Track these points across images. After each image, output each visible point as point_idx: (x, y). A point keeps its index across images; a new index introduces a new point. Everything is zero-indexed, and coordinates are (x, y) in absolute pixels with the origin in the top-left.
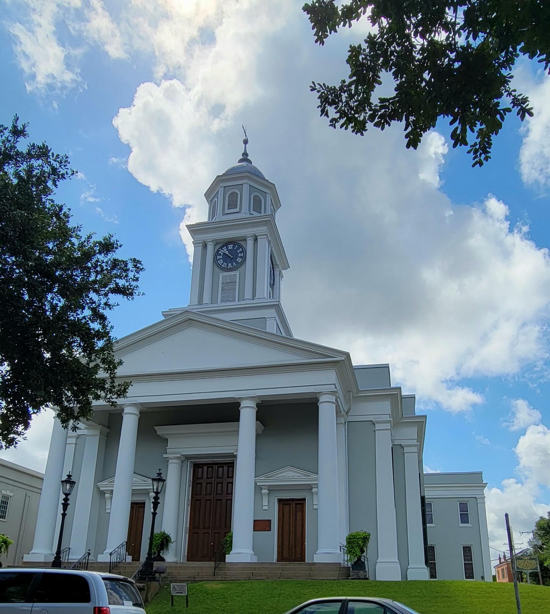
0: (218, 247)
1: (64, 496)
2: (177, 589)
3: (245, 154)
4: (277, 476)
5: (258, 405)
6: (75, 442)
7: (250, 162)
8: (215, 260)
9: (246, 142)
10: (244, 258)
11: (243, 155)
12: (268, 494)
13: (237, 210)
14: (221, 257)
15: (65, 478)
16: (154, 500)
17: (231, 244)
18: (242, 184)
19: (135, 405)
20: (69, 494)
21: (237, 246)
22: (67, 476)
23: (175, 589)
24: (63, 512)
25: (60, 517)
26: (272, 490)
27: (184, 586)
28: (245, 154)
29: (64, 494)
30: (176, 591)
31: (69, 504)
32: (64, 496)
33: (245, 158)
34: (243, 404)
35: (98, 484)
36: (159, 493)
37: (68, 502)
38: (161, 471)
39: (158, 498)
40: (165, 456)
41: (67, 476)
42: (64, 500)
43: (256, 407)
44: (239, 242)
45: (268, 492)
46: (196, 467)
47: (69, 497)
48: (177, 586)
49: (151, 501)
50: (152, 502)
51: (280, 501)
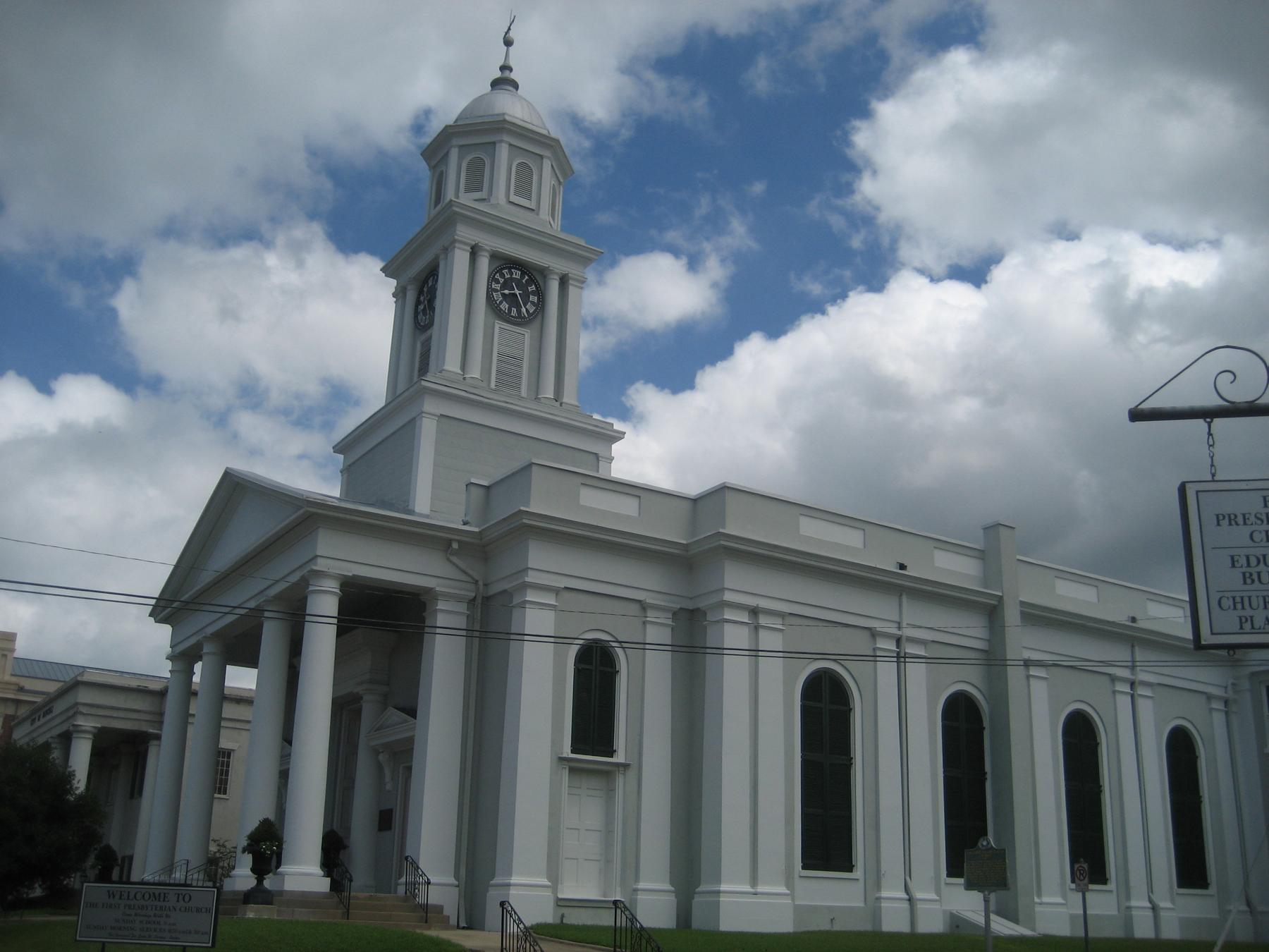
0: (497, 264)
10: (541, 305)
11: (503, 68)
13: (533, 205)
21: (527, 277)
27: (80, 937)
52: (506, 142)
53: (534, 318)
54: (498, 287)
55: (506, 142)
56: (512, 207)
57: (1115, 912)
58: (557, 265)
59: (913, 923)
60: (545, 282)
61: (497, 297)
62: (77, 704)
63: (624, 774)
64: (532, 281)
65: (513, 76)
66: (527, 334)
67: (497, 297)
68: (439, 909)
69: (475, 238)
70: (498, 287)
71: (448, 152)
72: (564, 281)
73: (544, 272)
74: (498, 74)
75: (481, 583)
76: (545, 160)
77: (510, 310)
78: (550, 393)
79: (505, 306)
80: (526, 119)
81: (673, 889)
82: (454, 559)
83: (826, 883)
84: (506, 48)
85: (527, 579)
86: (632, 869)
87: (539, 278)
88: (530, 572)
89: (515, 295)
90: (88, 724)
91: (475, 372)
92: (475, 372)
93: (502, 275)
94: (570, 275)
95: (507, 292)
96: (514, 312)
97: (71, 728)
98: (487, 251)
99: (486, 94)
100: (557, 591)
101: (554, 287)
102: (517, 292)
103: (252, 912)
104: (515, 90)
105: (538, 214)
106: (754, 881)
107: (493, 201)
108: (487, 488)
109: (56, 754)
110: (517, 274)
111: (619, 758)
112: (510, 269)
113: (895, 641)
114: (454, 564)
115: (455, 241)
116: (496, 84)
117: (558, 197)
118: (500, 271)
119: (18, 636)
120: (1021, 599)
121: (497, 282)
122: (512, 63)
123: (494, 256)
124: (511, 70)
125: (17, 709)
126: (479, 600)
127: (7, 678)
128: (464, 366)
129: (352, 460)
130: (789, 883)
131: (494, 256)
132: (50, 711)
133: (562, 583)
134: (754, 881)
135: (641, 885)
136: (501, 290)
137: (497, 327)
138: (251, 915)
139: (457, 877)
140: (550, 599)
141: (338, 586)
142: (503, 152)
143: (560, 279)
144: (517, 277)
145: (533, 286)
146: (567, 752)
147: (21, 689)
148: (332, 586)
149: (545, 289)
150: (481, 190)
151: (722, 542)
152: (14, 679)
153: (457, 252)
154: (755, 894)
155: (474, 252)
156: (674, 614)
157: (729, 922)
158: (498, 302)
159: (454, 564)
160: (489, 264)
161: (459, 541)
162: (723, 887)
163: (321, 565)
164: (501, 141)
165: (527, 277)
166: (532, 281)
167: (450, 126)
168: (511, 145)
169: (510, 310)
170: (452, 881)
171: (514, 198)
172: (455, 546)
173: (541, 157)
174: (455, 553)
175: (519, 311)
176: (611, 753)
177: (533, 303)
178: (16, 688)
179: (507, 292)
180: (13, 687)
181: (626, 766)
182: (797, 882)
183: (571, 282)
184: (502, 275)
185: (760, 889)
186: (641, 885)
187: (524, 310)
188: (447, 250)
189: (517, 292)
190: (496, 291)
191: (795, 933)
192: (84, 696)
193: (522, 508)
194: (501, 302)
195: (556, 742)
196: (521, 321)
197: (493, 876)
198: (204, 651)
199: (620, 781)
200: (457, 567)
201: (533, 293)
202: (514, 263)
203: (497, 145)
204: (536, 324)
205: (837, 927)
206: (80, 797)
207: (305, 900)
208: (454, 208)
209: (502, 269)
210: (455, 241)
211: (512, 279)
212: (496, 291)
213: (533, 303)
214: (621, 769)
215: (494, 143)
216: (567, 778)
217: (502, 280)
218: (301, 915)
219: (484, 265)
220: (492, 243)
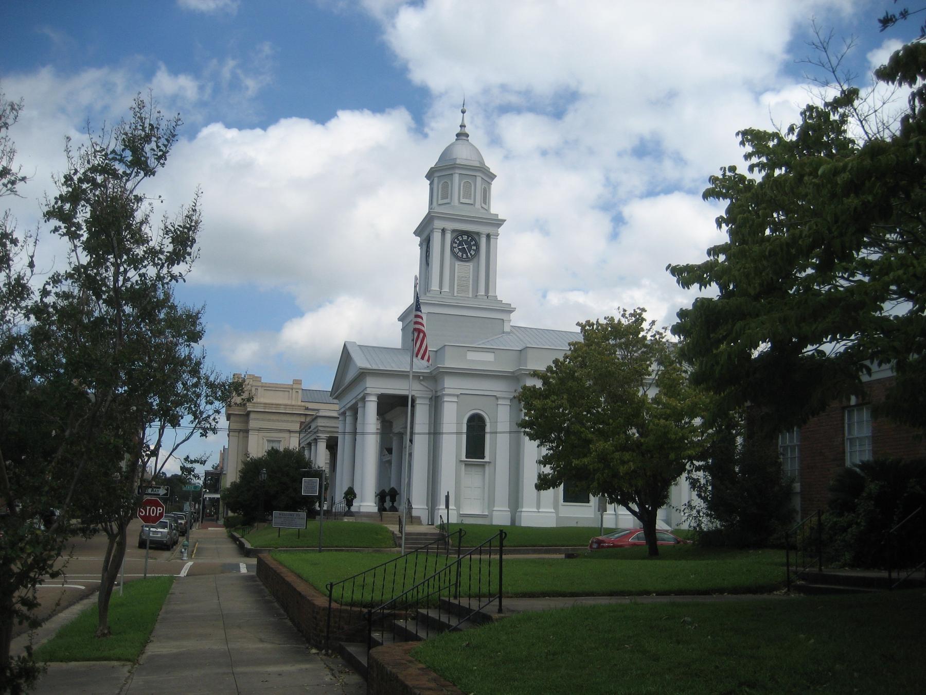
0: (455, 234)
3: (463, 126)
8: (452, 248)
10: (478, 250)
13: (471, 202)
21: (470, 238)
28: (463, 126)
38: (67, 136)
52: (457, 173)
53: (474, 257)
54: (456, 245)
55: (457, 173)
56: (462, 205)
57: (593, 516)
58: (484, 230)
59: (616, 524)
60: (479, 239)
61: (456, 250)
62: (317, 426)
63: (489, 465)
64: (473, 239)
65: (467, 130)
66: (470, 265)
67: (456, 250)
68: (419, 518)
70: (456, 245)
71: (433, 180)
72: (488, 236)
73: (478, 234)
74: (458, 130)
75: (434, 391)
76: (477, 177)
77: (462, 255)
78: (482, 292)
79: (460, 254)
80: (469, 158)
81: (509, 510)
82: (422, 383)
83: (580, 507)
85: (444, 392)
86: (491, 502)
88: (446, 389)
89: (464, 248)
90: (323, 436)
91: (446, 289)
92: (446, 289)
93: (458, 240)
95: (460, 247)
96: (465, 256)
97: (316, 437)
99: (452, 145)
100: (458, 396)
101: (483, 240)
102: (465, 246)
103: (346, 520)
104: (466, 138)
105: (474, 206)
106: (538, 506)
107: (452, 204)
108: (436, 351)
109: (306, 453)
110: (465, 237)
111: (487, 459)
112: (461, 236)
114: (422, 384)
115: (434, 229)
116: (458, 135)
119: (413, 231)
121: (456, 243)
123: (454, 231)
124: (465, 126)
125: (306, 418)
126: (433, 398)
127: (300, 403)
128: (441, 286)
129: (406, 323)
130: (556, 507)
132: (310, 427)
133: (459, 392)
134: (538, 506)
135: (495, 509)
136: (458, 247)
137: (456, 264)
138: (346, 520)
139: (427, 505)
140: (455, 399)
141: (377, 398)
142: (456, 178)
143: (487, 236)
146: (464, 458)
147: (307, 409)
148: (375, 399)
149: (480, 241)
150: (447, 198)
151: (523, 372)
152: (303, 404)
153: (435, 234)
154: (539, 512)
155: (443, 231)
156: (511, 400)
157: (524, 524)
159: (422, 384)
161: (423, 376)
162: (523, 510)
163: (368, 391)
164: (455, 173)
165: (470, 238)
167: (433, 168)
168: (482, 178)
169: (462, 255)
170: (426, 507)
171: (463, 200)
172: (421, 378)
174: (421, 380)
175: (467, 255)
176: (483, 457)
177: (474, 250)
178: (304, 408)
179: (460, 247)
180: (302, 408)
181: (489, 462)
182: (560, 507)
183: (492, 237)
184: (458, 240)
185: (540, 510)
186: (495, 509)
187: (469, 254)
188: (432, 231)
189: (465, 246)
190: (455, 247)
191: (556, 527)
192: (320, 422)
193: (439, 366)
194: (458, 252)
195: (458, 454)
196: (468, 260)
197: (437, 506)
198: (359, 406)
199: (487, 467)
200: (424, 386)
201: (474, 245)
203: (454, 175)
204: (475, 260)
205: (579, 525)
207: (368, 515)
208: (432, 214)
209: (457, 237)
210: (434, 229)
211: (463, 240)
212: (455, 247)
213: (474, 250)
214: (488, 464)
215: (452, 174)
216: (464, 470)
217: (458, 242)
218: (365, 520)
219: (449, 237)
220: (450, 226)
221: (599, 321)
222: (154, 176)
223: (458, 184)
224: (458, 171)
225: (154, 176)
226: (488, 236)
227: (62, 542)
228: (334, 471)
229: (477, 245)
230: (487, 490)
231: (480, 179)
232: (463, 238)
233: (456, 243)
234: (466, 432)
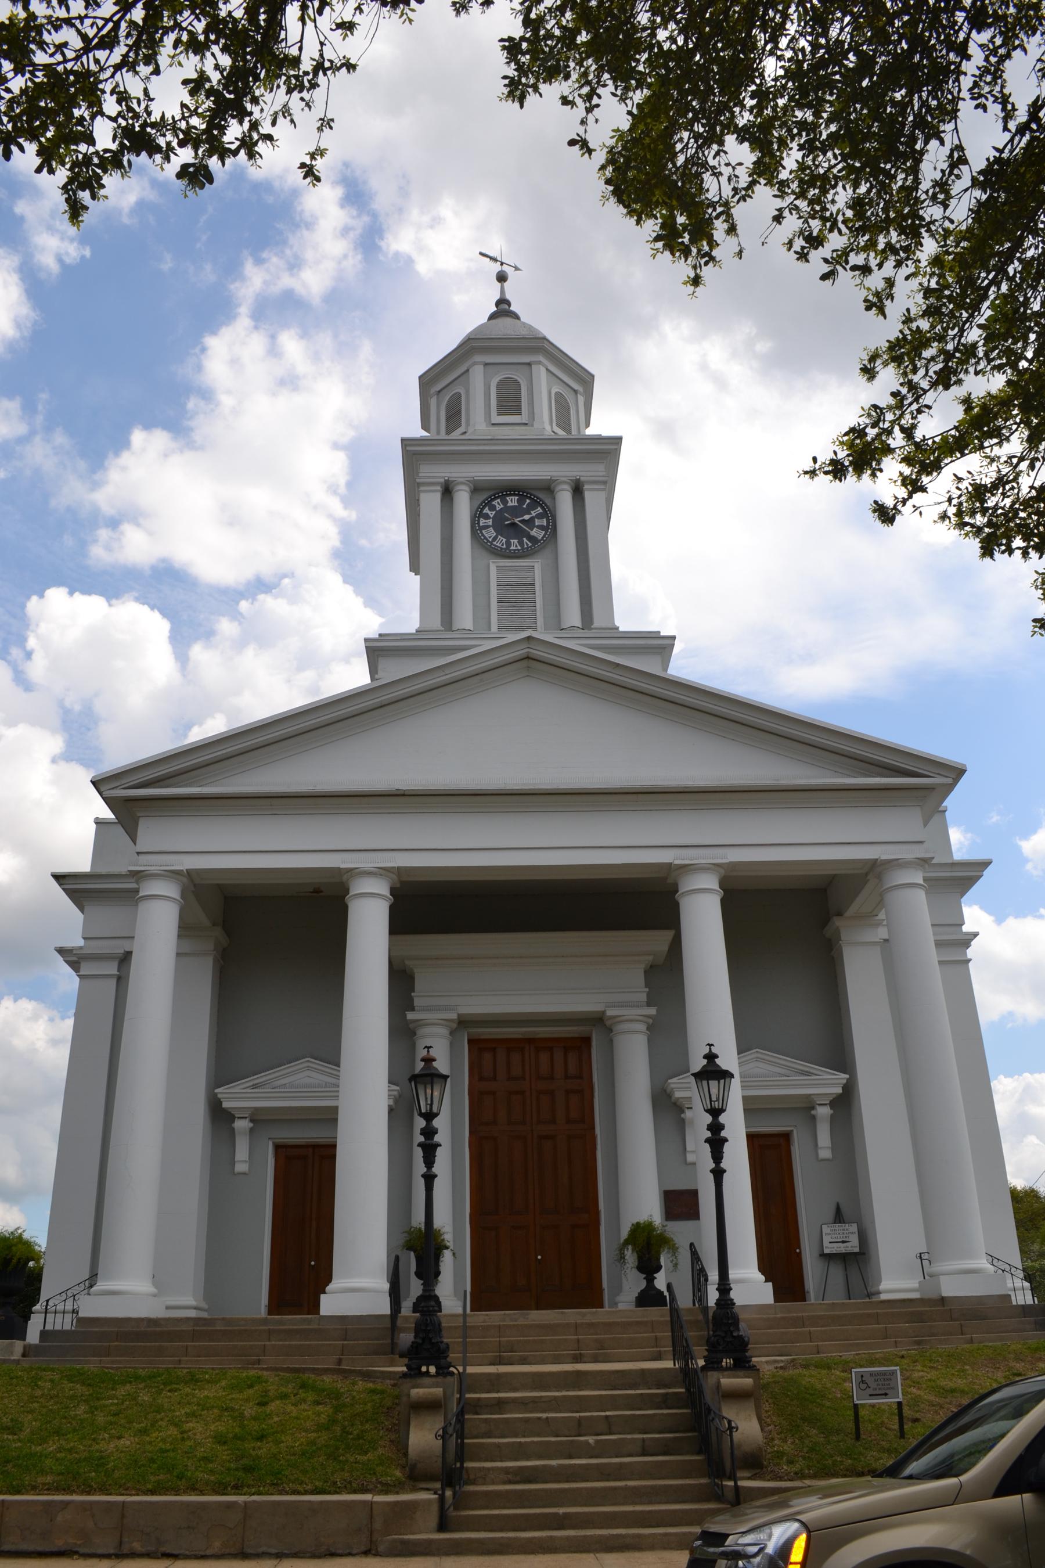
0: (483, 497)
1: (708, 1119)
2: (873, 1385)
3: (502, 302)
4: (283, 1082)
5: (393, 891)
6: (116, 972)
7: (516, 317)
8: (476, 531)
9: (502, 278)
10: (552, 529)
11: (498, 303)
12: (251, 1130)
13: (523, 418)
14: (490, 522)
15: (698, 1063)
16: (709, 1134)
17: (515, 495)
18: (529, 364)
19: (174, 875)
20: (721, 1111)
21: (528, 501)
22: (705, 1057)
23: (863, 1386)
24: (714, 1165)
25: (420, 1185)
26: (260, 1119)
27: (893, 1373)
29: (707, 1111)
30: (870, 1391)
31: (726, 1140)
32: (708, 1119)
33: (503, 309)
34: (361, 886)
35: (216, 1091)
36: (437, 1115)
37: (723, 1134)
38: (714, 1050)
39: (722, 1127)
40: (410, 1016)
41: (705, 1057)
42: (710, 1128)
43: (179, 898)
44: (533, 492)
45: (251, 1125)
46: (474, 1043)
47: (722, 1119)
48: (872, 1374)
49: (416, 1143)
50: (420, 1145)
51: (278, 1148)
58: (562, 472)
66: (537, 565)
69: (443, 475)
72: (578, 490)
73: (549, 487)
78: (573, 616)
84: (499, 284)
87: (541, 495)
94: (582, 478)
98: (564, 482)
113: (638, 979)
117: (572, 412)
118: (488, 503)
120: (263, 1312)
122: (508, 297)
123: (476, 488)
124: (509, 304)
131: (476, 488)
144: (513, 504)
145: (539, 508)
148: (710, 882)
149: (555, 507)
155: (447, 491)
158: (519, 548)
160: (471, 499)
166: (536, 503)
173: (576, 392)
183: (586, 487)
202: (504, 490)
206: (1018, 850)
221: (1023, 53)
222: (717, 1057)
223: (482, 384)
224: (479, 358)
225: (717, 1057)
226: (578, 490)
227: (277, 1415)
228: (934, 789)
229: (550, 515)
230: (491, 584)
231: (543, 370)
232: (505, 502)
233: (487, 517)
234: (1019, 1496)
